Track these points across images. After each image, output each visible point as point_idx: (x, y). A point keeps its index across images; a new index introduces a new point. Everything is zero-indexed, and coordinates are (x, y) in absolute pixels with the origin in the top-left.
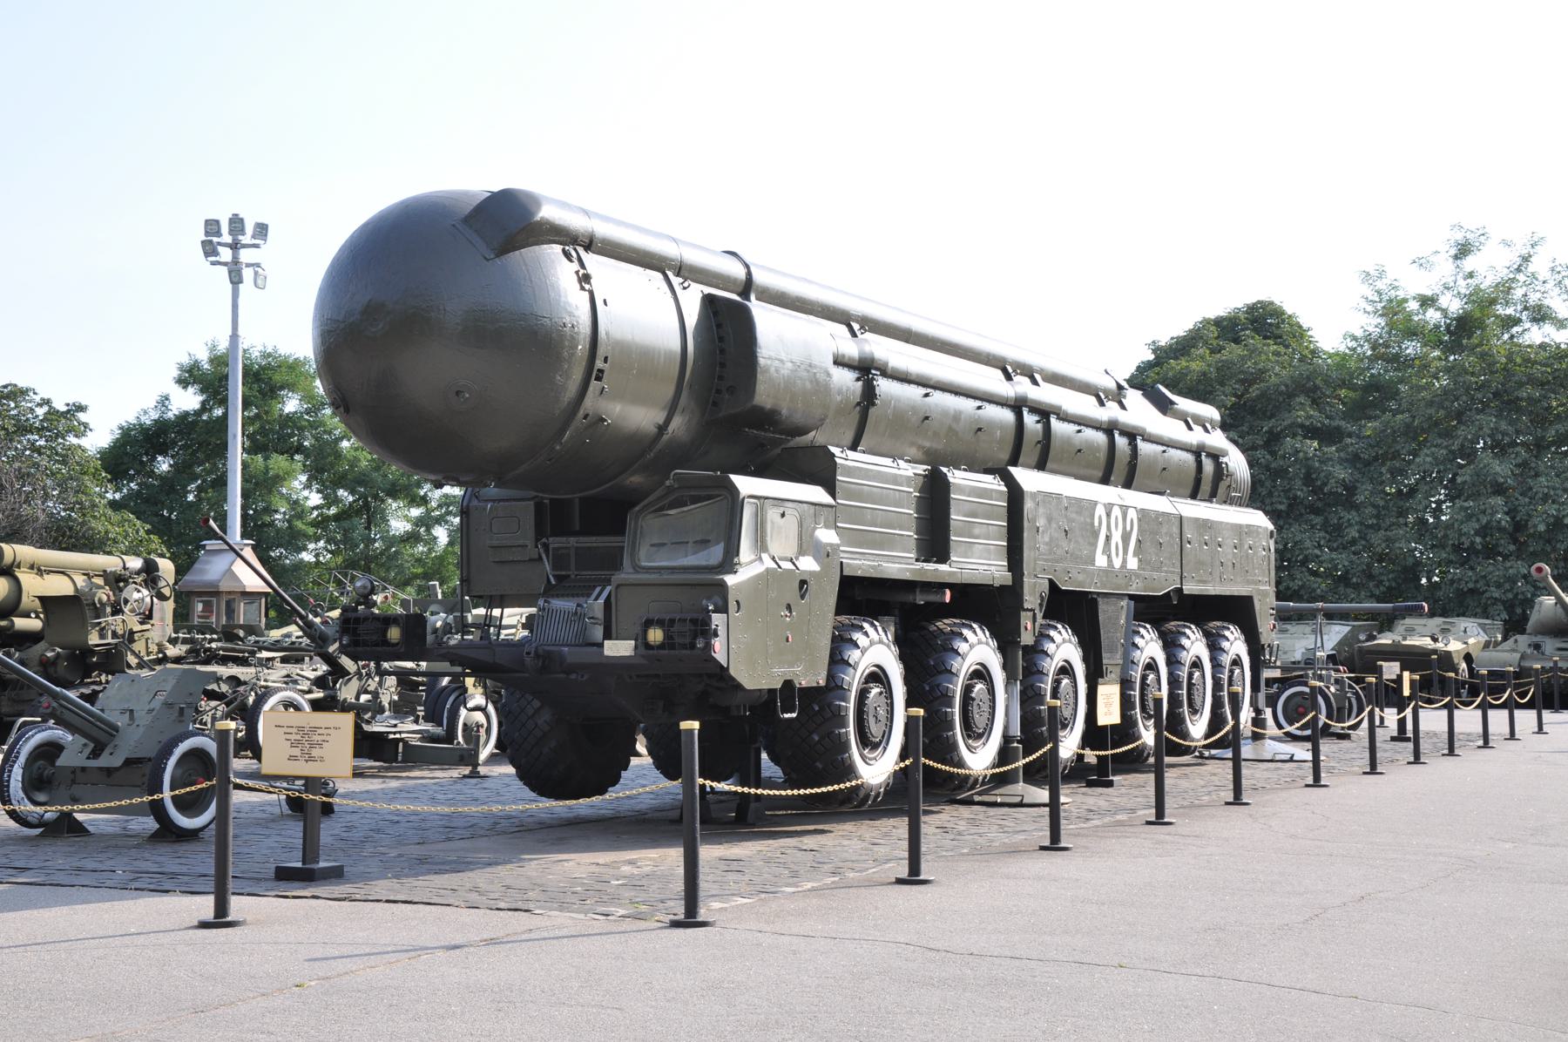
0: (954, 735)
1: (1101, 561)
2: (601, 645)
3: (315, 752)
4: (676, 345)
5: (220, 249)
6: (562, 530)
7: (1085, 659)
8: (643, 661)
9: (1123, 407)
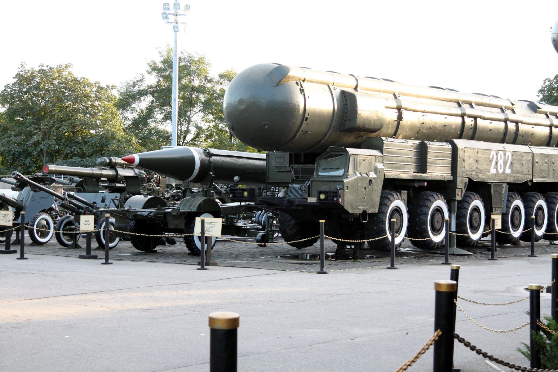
0: (385, 227)
1: (493, 171)
2: (307, 199)
3: (211, 229)
4: (332, 109)
5: (169, 16)
6: (297, 162)
7: (485, 207)
8: (318, 204)
9: (514, 112)
